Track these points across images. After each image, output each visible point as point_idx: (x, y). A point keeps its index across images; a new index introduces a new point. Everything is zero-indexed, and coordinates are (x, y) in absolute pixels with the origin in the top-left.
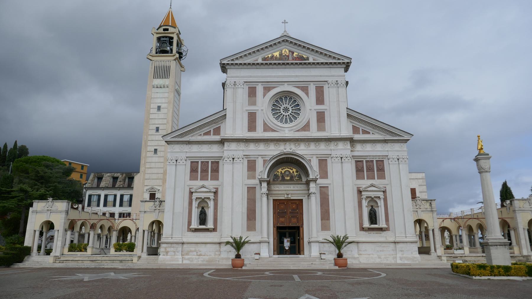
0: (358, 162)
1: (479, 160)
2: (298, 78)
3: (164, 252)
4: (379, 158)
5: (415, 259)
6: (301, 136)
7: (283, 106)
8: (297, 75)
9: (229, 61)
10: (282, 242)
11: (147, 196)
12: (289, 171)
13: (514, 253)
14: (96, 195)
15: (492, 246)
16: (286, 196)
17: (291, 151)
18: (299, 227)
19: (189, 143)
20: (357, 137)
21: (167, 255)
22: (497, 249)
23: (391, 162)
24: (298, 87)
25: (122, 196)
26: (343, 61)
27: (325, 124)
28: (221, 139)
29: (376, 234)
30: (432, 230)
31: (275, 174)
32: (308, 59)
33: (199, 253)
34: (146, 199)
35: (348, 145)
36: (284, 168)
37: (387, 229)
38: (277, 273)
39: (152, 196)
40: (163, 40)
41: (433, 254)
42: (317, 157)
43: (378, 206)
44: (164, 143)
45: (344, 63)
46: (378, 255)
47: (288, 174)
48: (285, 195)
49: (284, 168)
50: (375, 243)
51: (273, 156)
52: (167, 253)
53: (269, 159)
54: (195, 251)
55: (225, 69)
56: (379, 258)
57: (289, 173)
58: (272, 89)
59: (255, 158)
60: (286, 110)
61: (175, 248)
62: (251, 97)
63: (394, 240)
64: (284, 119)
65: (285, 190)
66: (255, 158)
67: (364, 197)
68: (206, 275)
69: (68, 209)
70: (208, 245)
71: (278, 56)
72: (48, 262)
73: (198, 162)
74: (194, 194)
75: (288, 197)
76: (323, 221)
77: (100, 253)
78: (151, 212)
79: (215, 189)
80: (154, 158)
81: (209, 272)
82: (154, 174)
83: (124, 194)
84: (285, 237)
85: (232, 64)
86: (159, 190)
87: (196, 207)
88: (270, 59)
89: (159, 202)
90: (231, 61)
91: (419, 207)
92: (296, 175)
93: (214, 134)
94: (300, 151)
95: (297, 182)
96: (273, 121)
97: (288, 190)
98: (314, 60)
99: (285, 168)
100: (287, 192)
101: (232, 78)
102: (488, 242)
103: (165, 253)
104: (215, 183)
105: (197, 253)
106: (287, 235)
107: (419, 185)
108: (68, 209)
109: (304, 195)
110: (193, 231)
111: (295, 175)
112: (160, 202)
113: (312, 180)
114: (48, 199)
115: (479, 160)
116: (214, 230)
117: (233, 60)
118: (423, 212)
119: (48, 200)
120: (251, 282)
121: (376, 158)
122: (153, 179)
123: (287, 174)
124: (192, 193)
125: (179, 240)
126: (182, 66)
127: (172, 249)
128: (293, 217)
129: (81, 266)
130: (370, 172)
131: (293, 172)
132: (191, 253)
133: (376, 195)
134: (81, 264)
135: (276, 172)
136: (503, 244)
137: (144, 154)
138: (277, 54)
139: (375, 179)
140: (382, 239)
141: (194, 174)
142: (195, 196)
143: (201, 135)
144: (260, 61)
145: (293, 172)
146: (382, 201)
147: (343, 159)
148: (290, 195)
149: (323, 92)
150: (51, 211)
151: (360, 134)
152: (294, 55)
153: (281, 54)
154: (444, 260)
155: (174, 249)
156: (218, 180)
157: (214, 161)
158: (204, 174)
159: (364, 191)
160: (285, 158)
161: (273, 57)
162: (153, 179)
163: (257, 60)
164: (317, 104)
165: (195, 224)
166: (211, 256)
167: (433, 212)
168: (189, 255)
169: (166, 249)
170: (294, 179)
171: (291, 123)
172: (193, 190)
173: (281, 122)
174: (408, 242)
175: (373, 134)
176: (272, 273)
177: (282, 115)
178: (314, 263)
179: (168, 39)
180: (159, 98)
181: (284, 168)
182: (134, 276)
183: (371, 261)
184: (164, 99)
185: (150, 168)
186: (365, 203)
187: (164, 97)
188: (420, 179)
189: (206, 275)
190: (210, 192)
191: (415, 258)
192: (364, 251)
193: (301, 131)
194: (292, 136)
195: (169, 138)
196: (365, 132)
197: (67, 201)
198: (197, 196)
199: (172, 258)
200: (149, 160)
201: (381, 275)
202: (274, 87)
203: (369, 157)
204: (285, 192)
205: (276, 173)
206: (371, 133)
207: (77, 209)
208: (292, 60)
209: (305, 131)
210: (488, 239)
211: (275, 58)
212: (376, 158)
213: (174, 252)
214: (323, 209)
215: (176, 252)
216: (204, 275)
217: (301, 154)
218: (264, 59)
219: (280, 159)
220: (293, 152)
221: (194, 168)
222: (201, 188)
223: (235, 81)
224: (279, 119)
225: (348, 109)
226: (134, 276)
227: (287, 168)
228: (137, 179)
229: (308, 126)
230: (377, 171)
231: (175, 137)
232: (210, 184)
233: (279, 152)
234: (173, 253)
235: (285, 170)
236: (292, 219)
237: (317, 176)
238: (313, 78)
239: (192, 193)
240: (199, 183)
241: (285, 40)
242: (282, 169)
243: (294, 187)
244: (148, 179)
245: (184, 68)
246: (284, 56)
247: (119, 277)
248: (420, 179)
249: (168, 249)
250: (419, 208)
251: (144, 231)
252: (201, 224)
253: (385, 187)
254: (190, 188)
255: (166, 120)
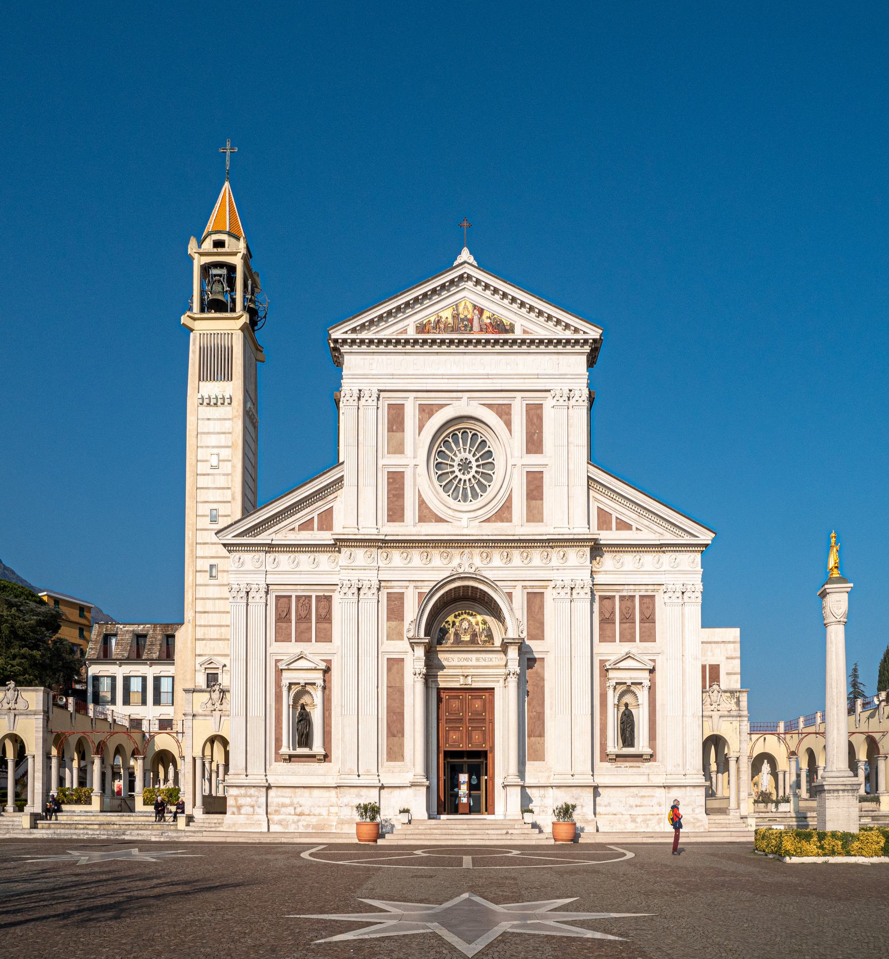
0: (605, 600)
1: (828, 593)
2: (491, 381)
3: (233, 806)
4: (647, 591)
5: (698, 824)
6: (495, 533)
7: (463, 453)
8: (490, 372)
9: (346, 332)
10: (454, 784)
11: (201, 681)
12: (470, 621)
13: (879, 811)
14: (107, 677)
15: (830, 793)
16: (462, 679)
17: (472, 571)
18: (486, 752)
19: (271, 548)
20: (606, 537)
21: (240, 814)
22: (838, 798)
23: (669, 601)
24: (489, 406)
25: (127, 680)
26: (586, 337)
27: (542, 504)
28: (334, 539)
29: (630, 769)
30: (736, 759)
31: (441, 629)
32: (512, 330)
33: (299, 810)
34: (201, 686)
35: (578, 557)
36: (460, 612)
37: (652, 757)
38: (438, 852)
39: (212, 679)
40: (215, 275)
41: (733, 815)
42: (524, 587)
43: (638, 705)
44: (224, 552)
45: (586, 341)
46: (630, 815)
47: (467, 628)
48: (461, 677)
49: (459, 614)
50: (623, 789)
51: (438, 583)
52: (239, 807)
53: (427, 591)
54: (291, 805)
55: (340, 356)
56: (632, 821)
57: (469, 624)
58: (437, 411)
59: (401, 587)
60: (465, 466)
61: (254, 799)
62: (393, 431)
63: (664, 781)
64: (469, 489)
65: (461, 667)
66: (401, 587)
67: (613, 683)
68: (305, 855)
69: (48, 708)
70: (316, 792)
71: (450, 320)
72: (21, 827)
73: (291, 596)
74: (285, 674)
75: (467, 683)
76: (532, 738)
77: (119, 809)
78: (205, 715)
79: (325, 664)
80: (211, 588)
81: (313, 850)
82: (212, 628)
83: (161, 677)
84: (462, 772)
85: (353, 342)
86: (225, 666)
87: (615, 704)
88: (433, 328)
89: (220, 693)
90: (352, 333)
91: (716, 706)
92: (483, 630)
93: (320, 529)
94: (491, 572)
95: (483, 647)
96: (438, 500)
97: (466, 667)
98: (525, 332)
99: (462, 614)
100: (464, 670)
101: (355, 381)
102: (824, 783)
103: (235, 810)
104: (323, 647)
105: (295, 808)
106: (465, 768)
107: (727, 658)
108: (48, 708)
109: (496, 679)
110: (285, 760)
111: (481, 631)
112: (222, 694)
113: (511, 643)
114: (7, 683)
115: (828, 593)
116: (326, 757)
117: (354, 330)
118: (722, 719)
119: (7, 685)
120: (380, 869)
121: (640, 590)
122: (211, 640)
123: (465, 629)
124: (607, 670)
125: (258, 781)
126: (259, 348)
127: (248, 799)
128: (475, 729)
129: (82, 837)
130: (628, 624)
131: (477, 624)
132: (283, 810)
133: (635, 678)
134: (81, 831)
135: (444, 623)
136: (849, 788)
137: (191, 578)
138: (447, 315)
139: (635, 641)
140: (642, 780)
141: (284, 625)
142: (287, 679)
143: (293, 529)
144: (411, 334)
145: (477, 624)
146: (320, 689)
147: (574, 592)
148: (470, 678)
149: (540, 418)
150: (16, 712)
151: (611, 529)
152: (484, 317)
153: (455, 316)
154: (751, 825)
155: (252, 801)
156: (331, 642)
157: (322, 594)
158: (303, 626)
159: (612, 669)
160: (461, 589)
161: (438, 321)
162: (211, 640)
163: (405, 331)
164: (529, 451)
165: (614, 746)
166: (321, 817)
167: (741, 719)
168: (279, 814)
169: (236, 800)
170: (479, 641)
171: (462, 503)
172: (282, 666)
173: (465, 501)
174: (688, 786)
175: (637, 529)
176: (428, 852)
177: (462, 482)
178: (510, 831)
179: (224, 271)
180: (213, 433)
181: (460, 612)
182: (173, 856)
183: (618, 828)
184: (223, 436)
185: (205, 612)
186: (612, 699)
187: (223, 431)
188: (729, 642)
189: (305, 855)
190: (315, 669)
191: (698, 820)
192: (606, 806)
193: (495, 521)
194: (476, 533)
195: (229, 537)
196: (623, 526)
197: (42, 688)
198: (290, 679)
199: (248, 819)
200: (201, 592)
201: (625, 855)
202: (442, 406)
203: (626, 587)
204: (461, 671)
205: (444, 626)
206: (634, 528)
207: (65, 707)
208: (478, 333)
209: (502, 521)
210: (825, 778)
211: (442, 326)
212: (640, 590)
213: (253, 806)
214: (532, 712)
215: (256, 808)
216: (302, 855)
217: (492, 579)
218: (421, 328)
219: (451, 590)
220: (476, 574)
221: (283, 611)
222: (298, 659)
223: (570, 388)
224: (451, 491)
225: (589, 466)
226: (173, 856)
227: (465, 613)
228: (182, 637)
229: (508, 507)
230: (642, 621)
231: (243, 534)
232: (315, 651)
233: (448, 574)
234: (250, 810)
235: (460, 618)
236: (451, 733)
237: (522, 633)
238: (446, 381)
239: (607, 670)
240: (293, 648)
241: (465, 275)
242: (456, 617)
243: (152, 656)
244: (203, 640)
245: (262, 352)
246: (462, 320)
247: (145, 858)
248: (729, 642)
249: (241, 801)
250: (715, 710)
251: (194, 759)
252: (301, 745)
253: (654, 661)
254: (277, 661)
255: (229, 491)
